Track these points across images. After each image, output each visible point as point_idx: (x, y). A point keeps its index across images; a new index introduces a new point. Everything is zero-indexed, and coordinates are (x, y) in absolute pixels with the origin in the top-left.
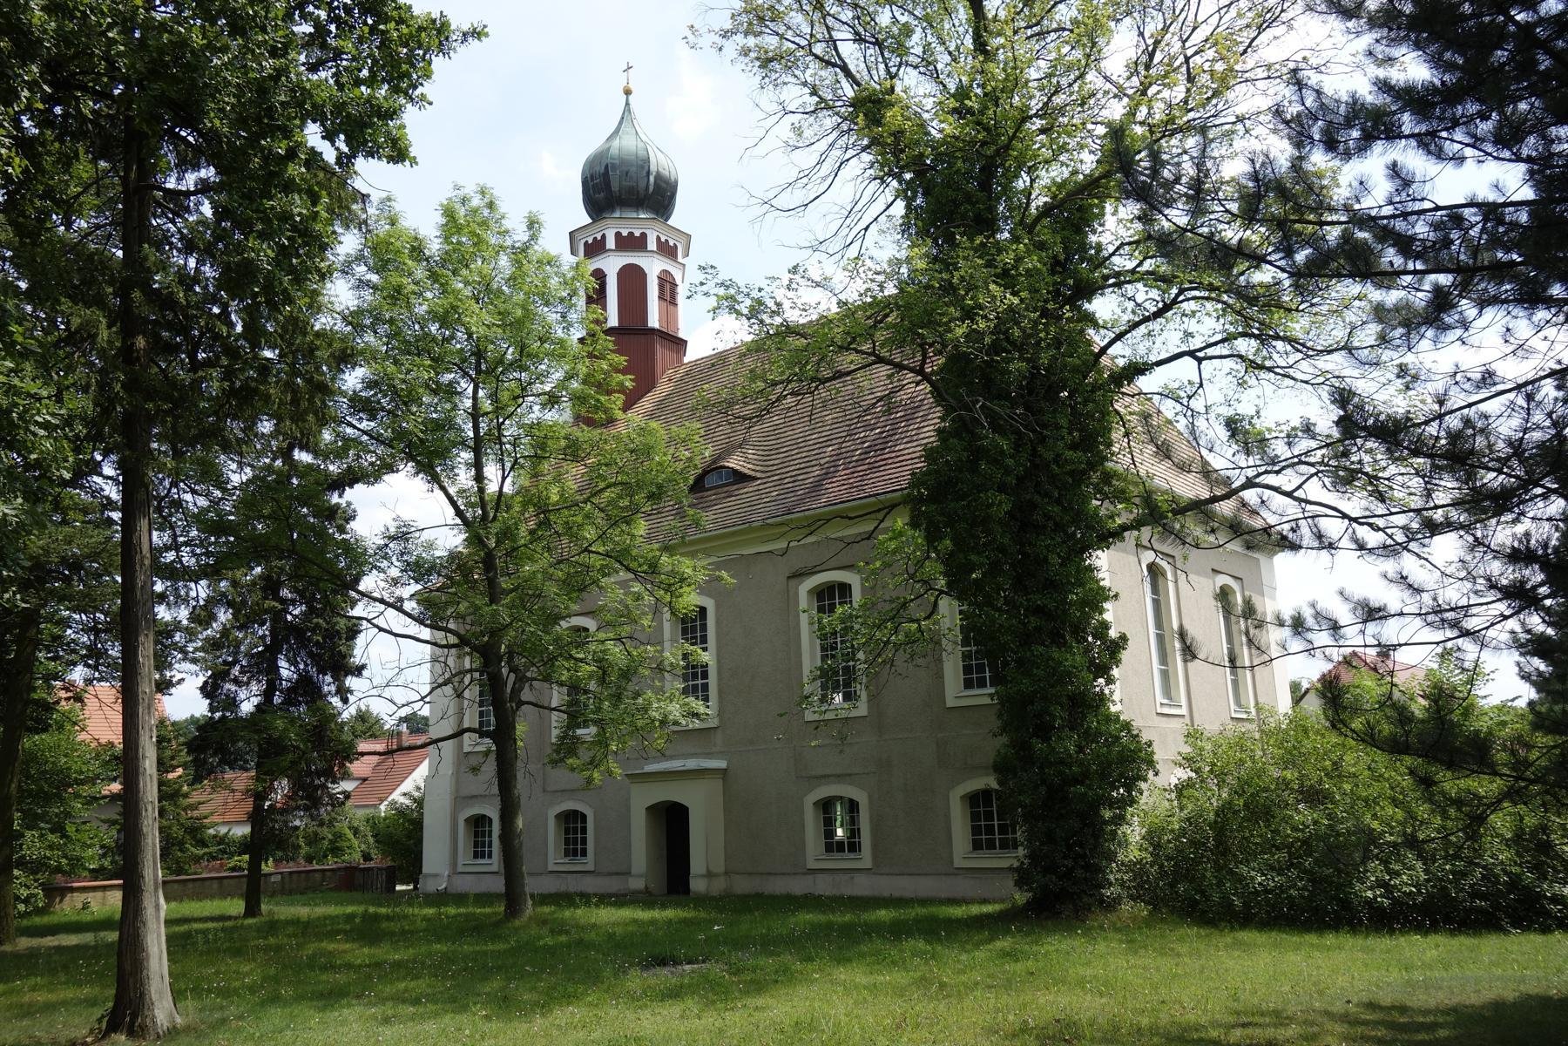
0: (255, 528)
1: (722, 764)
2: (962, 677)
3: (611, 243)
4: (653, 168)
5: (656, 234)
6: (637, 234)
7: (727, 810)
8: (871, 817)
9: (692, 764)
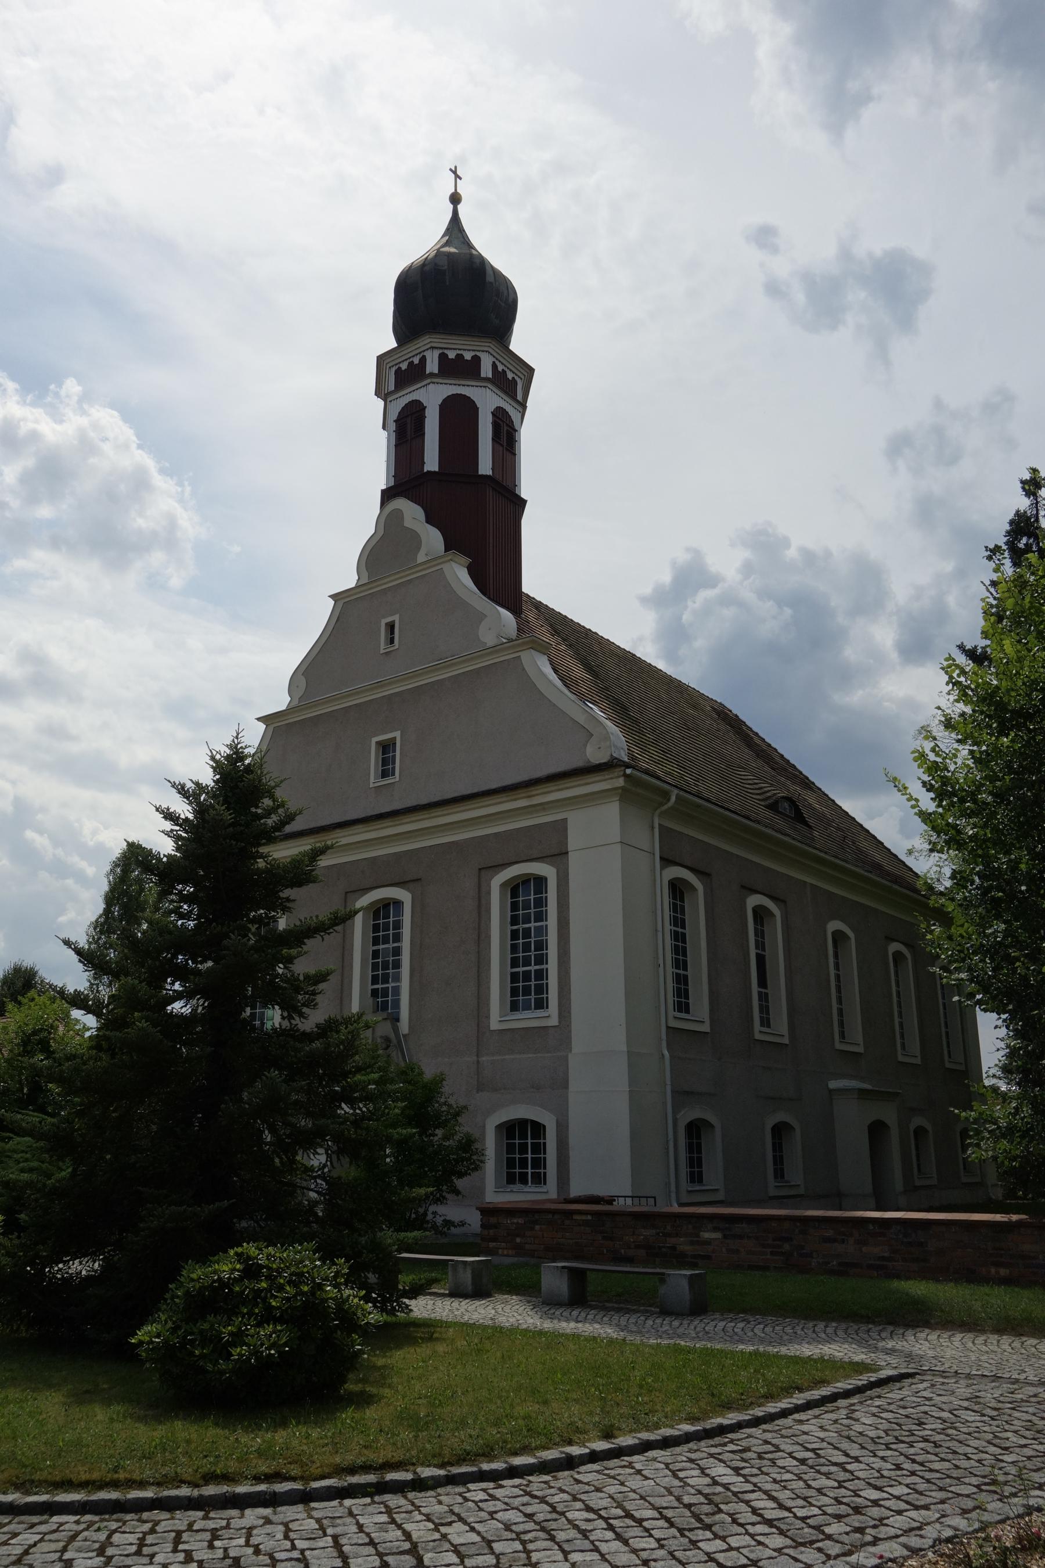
0: (1019, 1190)
3: (432, 366)
6: (468, 356)
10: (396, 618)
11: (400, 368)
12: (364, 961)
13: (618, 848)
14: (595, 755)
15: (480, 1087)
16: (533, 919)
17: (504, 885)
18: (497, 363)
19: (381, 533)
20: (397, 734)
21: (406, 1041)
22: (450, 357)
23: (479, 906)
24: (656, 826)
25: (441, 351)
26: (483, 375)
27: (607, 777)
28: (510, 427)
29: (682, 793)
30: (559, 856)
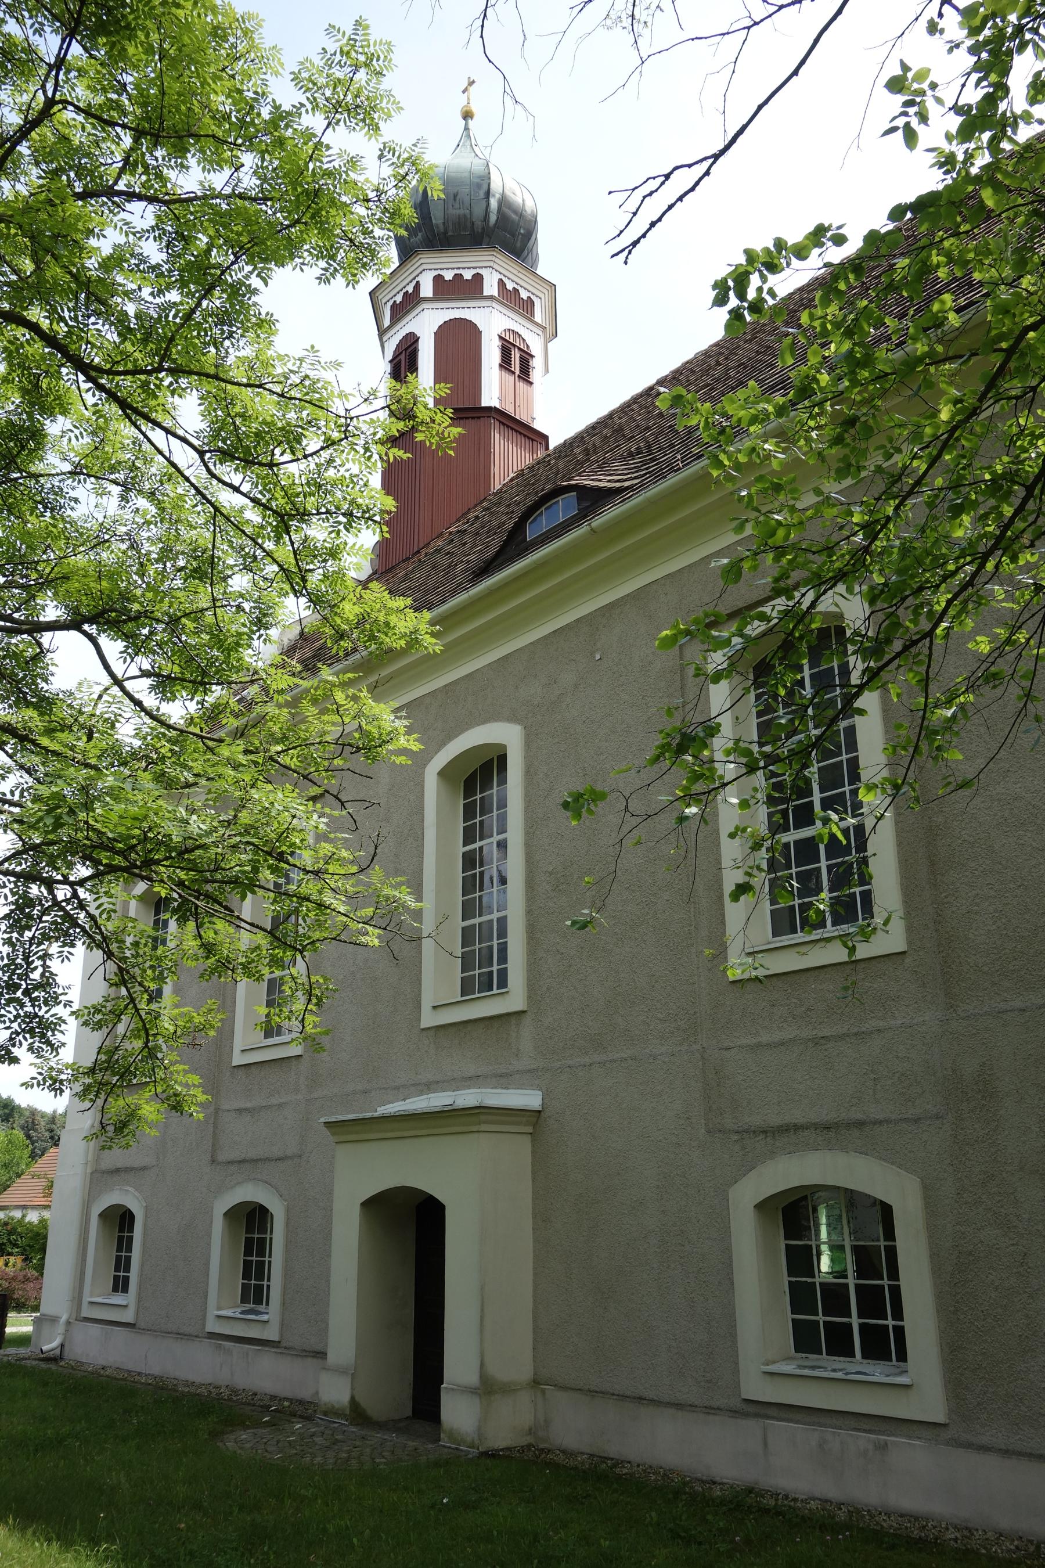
1: (530, 1099)
2: (786, 1279)
3: (427, 290)
4: (496, 185)
5: (496, 277)
6: (468, 275)
7: (541, 1217)
8: (935, 1255)
9: (468, 1098)
16: (809, 1280)
18: (505, 279)
22: (446, 278)
25: (436, 273)
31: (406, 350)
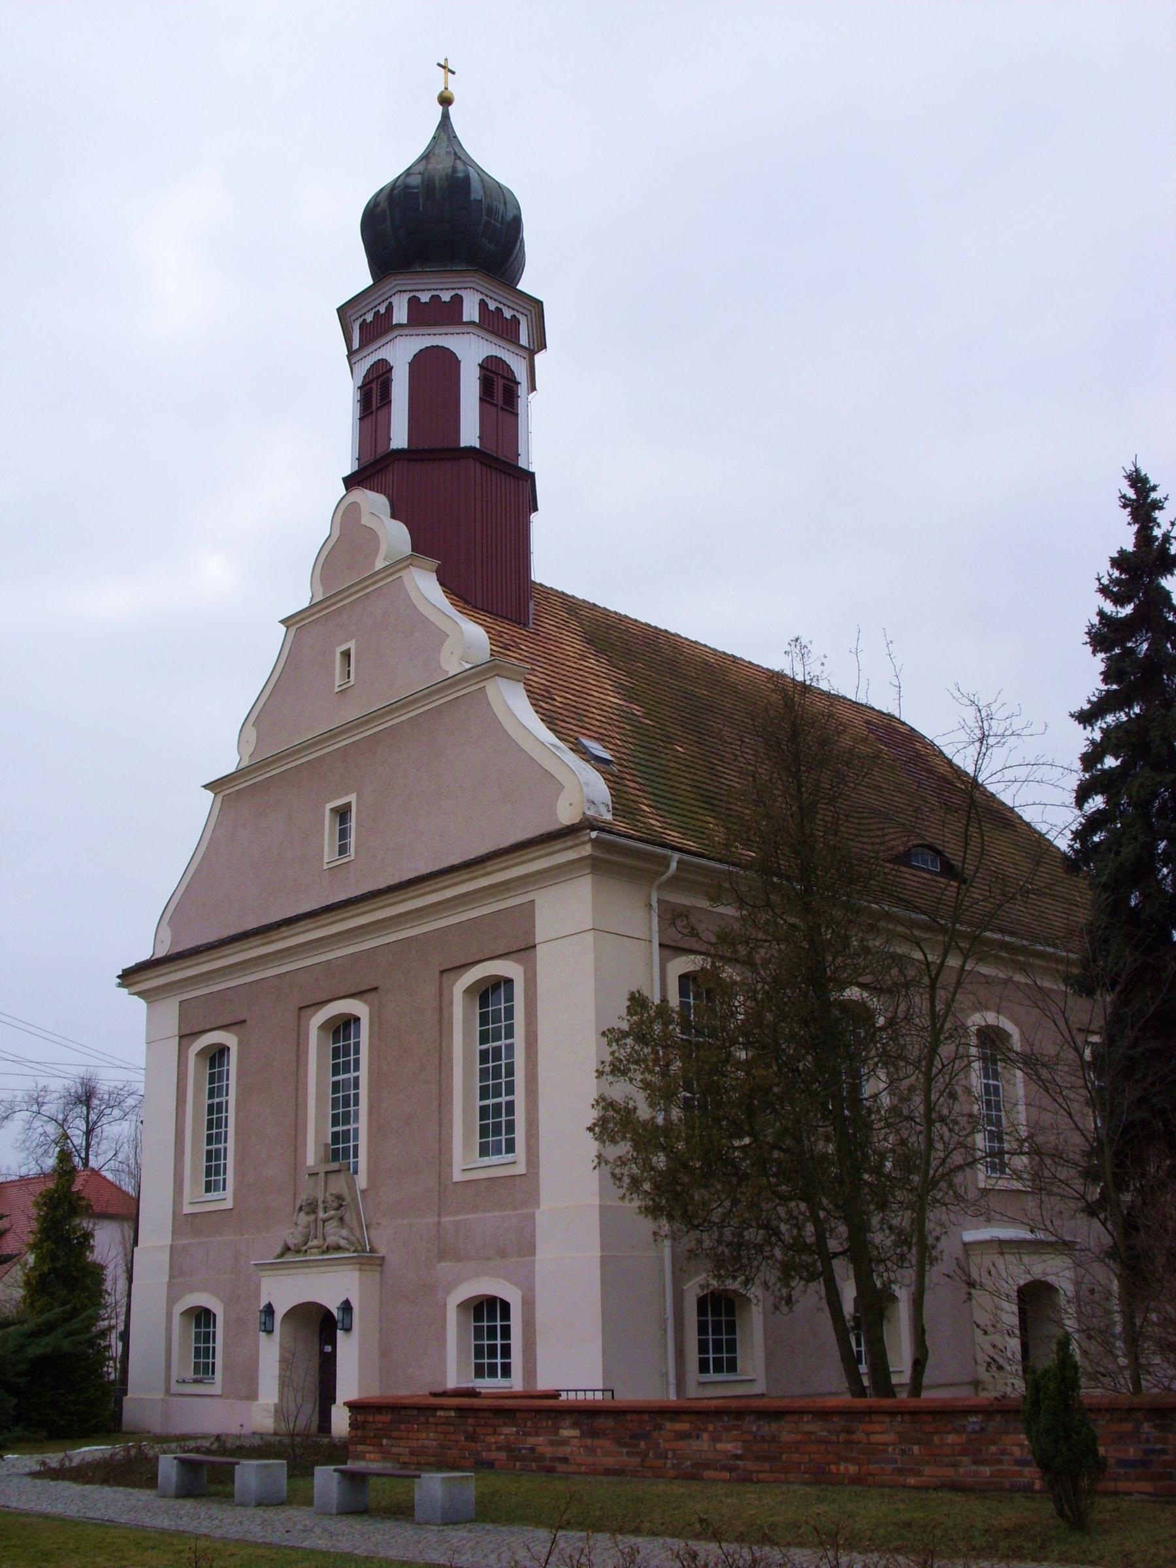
3: (400, 315)
6: (446, 297)
10: (351, 645)
11: (364, 320)
12: (319, 1097)
13: (590, 937)
14: (566, 815)
15: (442, 1255)
17: (468, 991)
18: (488, 300)
19: (337, 533)
20: (352, 798)
21: (364, 1199)
23: (440, 1021)
24: (655, 904)
25: (412, 294)
26: (465, 319)
27: (569, 844)
28: (509, 379)
29: (686, 857)
30: (525, 950)
31: (378, 377)
